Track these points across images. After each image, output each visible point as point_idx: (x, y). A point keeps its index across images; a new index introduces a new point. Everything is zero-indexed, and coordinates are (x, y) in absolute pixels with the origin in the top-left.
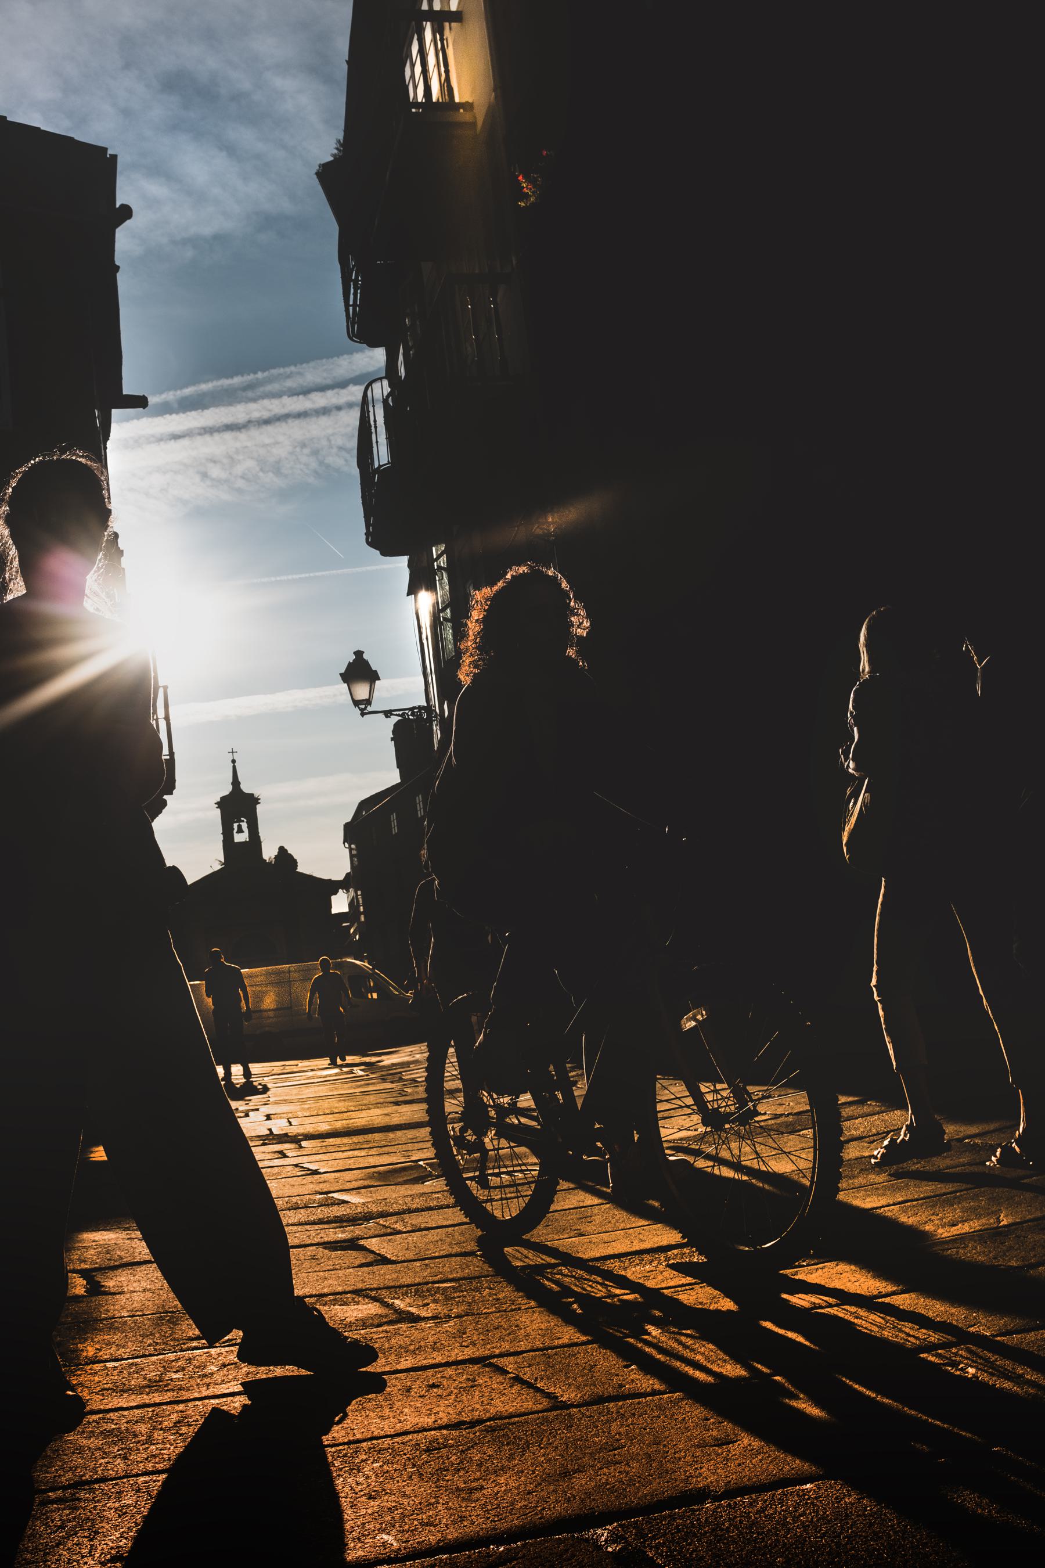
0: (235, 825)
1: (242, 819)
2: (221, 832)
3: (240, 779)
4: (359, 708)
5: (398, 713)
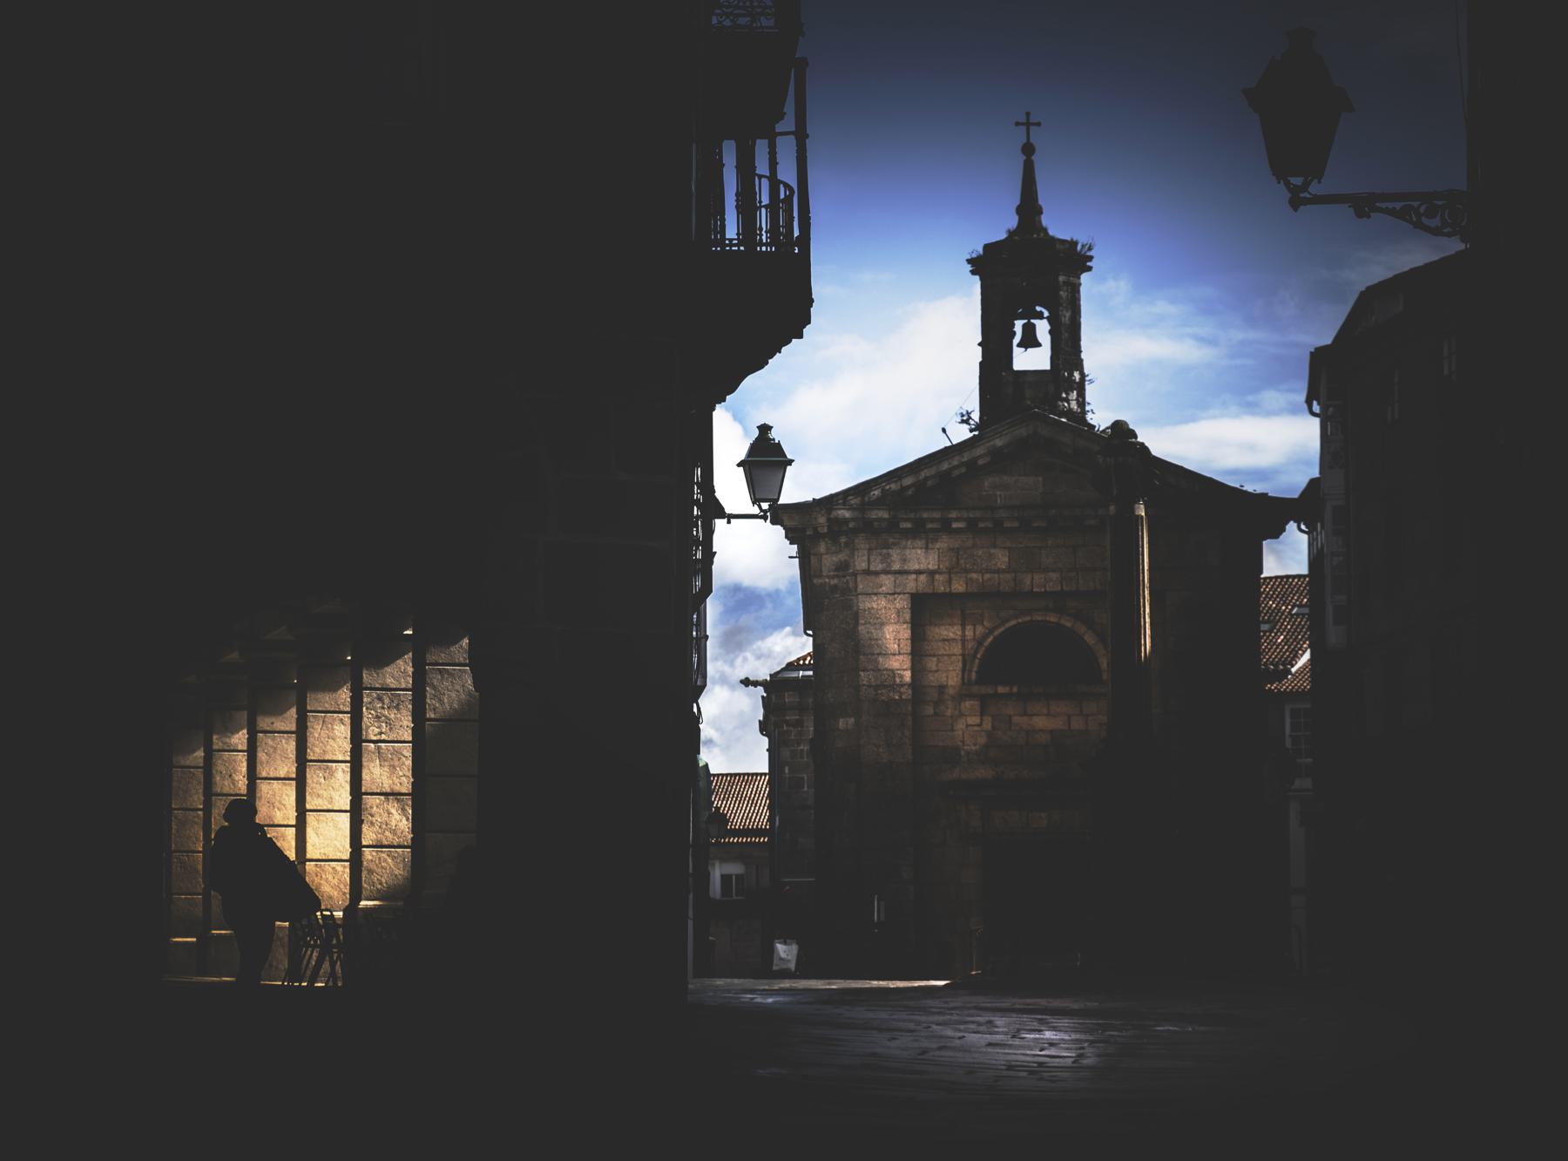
0: (1019, 325)
1: (1038, 309)
2: (980, 339)
3: (1042, 201)
4: (1287, 184)
5: (1390, 205)
